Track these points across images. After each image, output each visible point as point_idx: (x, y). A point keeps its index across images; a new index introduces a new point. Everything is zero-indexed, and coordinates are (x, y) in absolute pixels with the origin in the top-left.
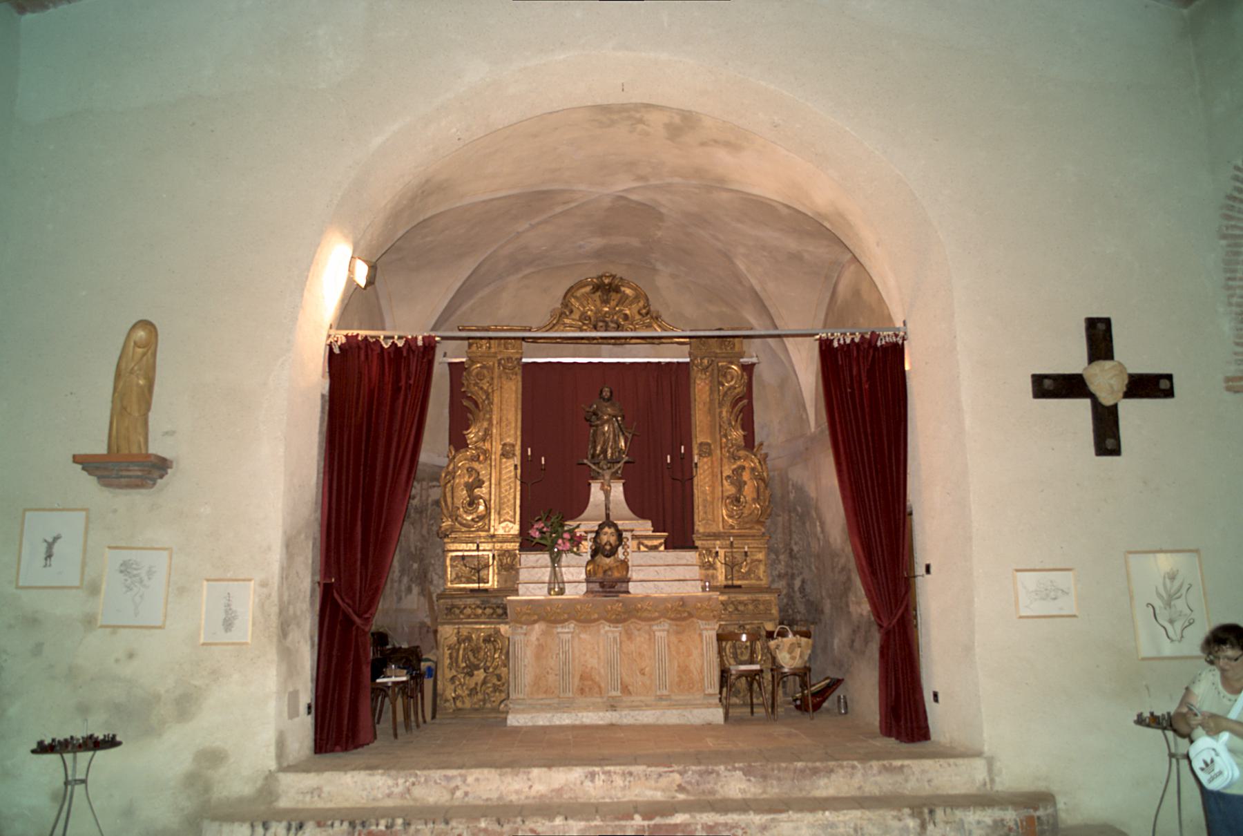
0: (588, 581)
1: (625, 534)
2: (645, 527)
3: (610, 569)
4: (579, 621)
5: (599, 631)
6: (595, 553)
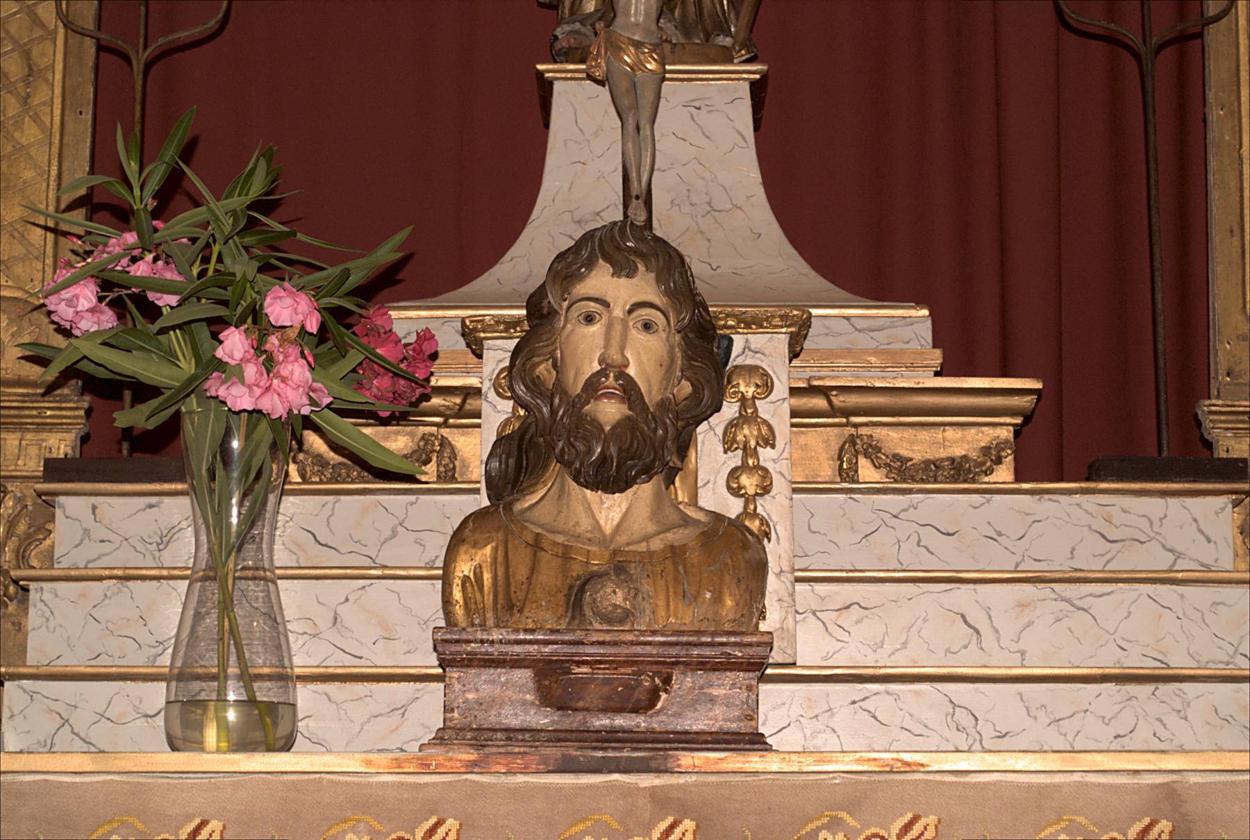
0: (453, 657)
2: (887, 339)
3: (619, 566)
6: (519, 460)
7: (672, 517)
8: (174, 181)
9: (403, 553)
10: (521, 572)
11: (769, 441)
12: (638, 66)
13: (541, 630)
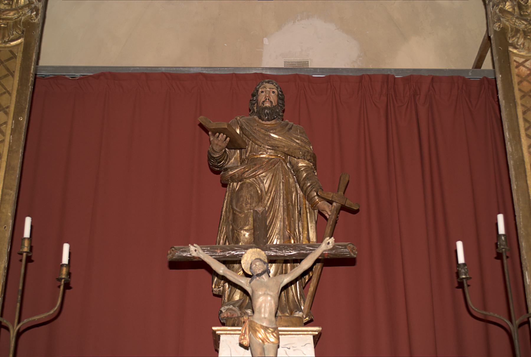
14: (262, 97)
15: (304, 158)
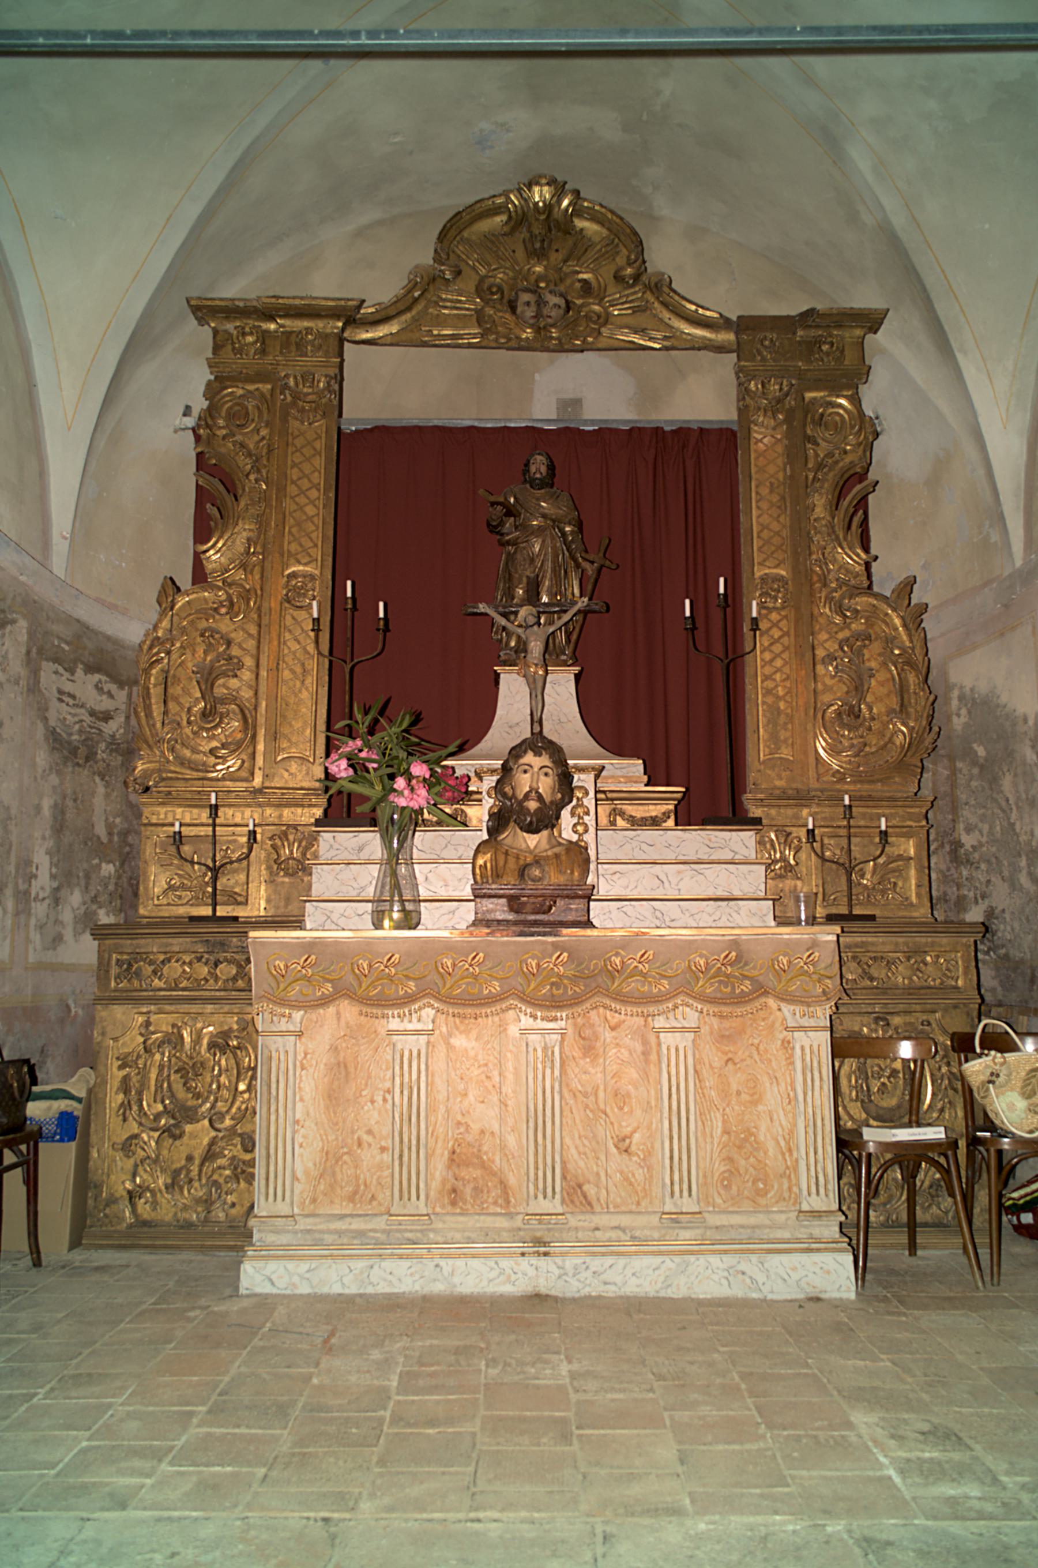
0: (478, 895)
1: (578, 779)
2: (627, 772)
3: (537, 862)
4: (448, 999)
5: (502, 1028)
6: (498, 822)
7: (554, 842)
8: (376, 721)
9: (450, 853)
10: (501, 863)
11: (587, 813)
12: (536, 673)
13: (509, 884)
14: (533, 469)
15: (570, 524)
